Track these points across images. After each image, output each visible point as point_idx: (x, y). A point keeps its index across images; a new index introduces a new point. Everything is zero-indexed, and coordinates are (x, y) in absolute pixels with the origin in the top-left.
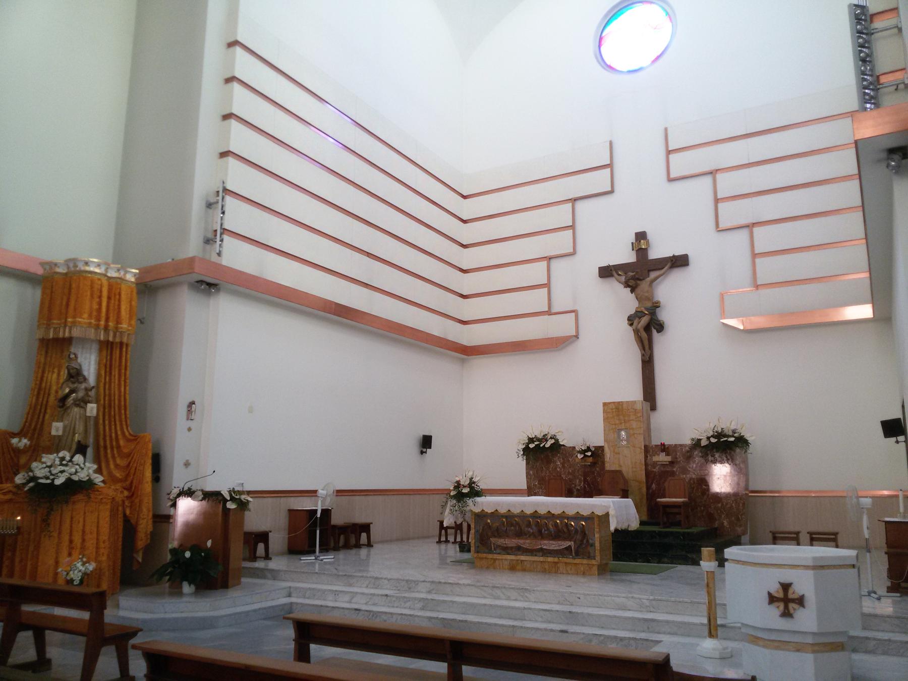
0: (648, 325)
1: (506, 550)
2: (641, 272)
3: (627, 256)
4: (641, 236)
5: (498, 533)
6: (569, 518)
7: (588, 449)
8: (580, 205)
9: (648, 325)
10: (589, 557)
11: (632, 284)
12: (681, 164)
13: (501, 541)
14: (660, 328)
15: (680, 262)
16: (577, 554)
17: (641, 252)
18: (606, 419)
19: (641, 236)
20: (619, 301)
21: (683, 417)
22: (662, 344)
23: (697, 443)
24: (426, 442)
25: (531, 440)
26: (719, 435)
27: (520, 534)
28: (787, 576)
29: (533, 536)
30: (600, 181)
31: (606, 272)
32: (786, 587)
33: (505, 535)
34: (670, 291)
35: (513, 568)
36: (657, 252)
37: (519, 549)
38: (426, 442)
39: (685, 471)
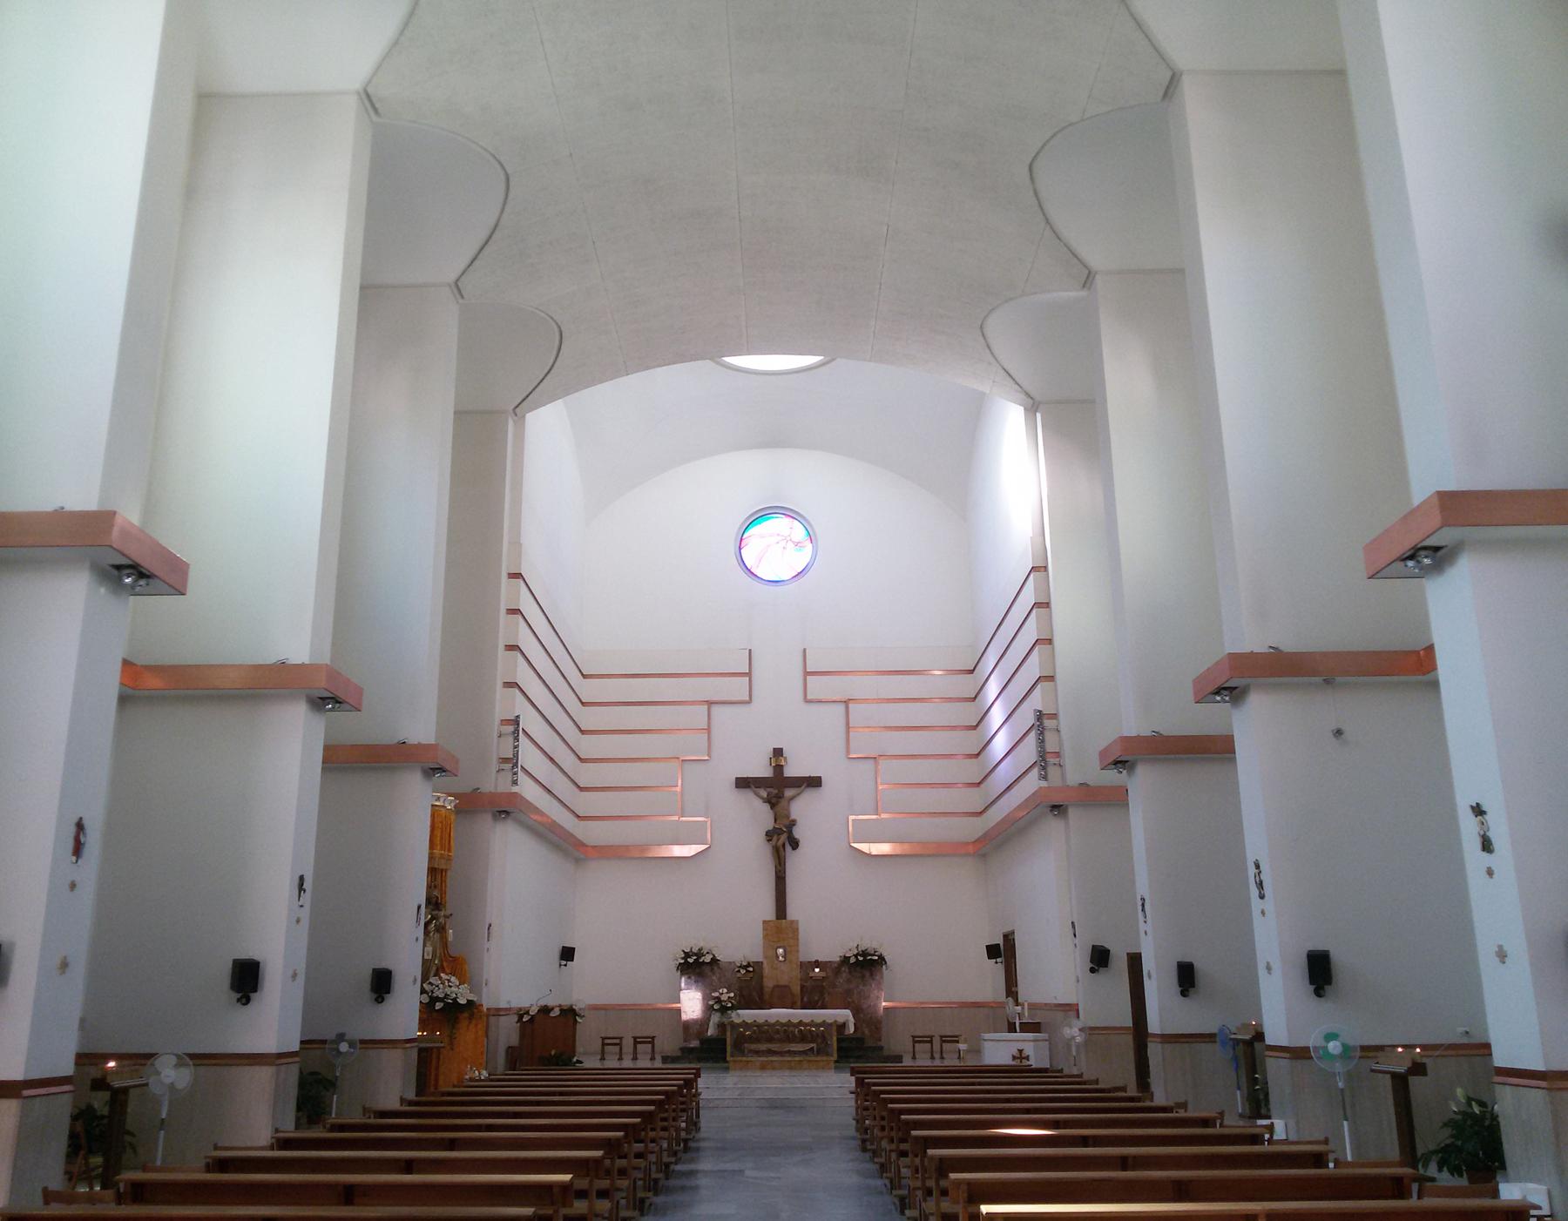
0: (783, 839)
1: (757, 1053)
2: (777, 787)
3: (762, 770)
4: (778, 752)
5: (751, 1039)
6: (806, 1025)
7: (749, 965)
8: (716, 709)
9: (783, 839)
10: (828, 1055)
11: (774, 802)
12: (817, 686)
13: (753, 1046)
14: (795, 844)
15: (814, 782)
16: (819, 1052)
17: (779, 769)
18: (765, 936)
19: (778, 752)
20: (754, 814)
21: (825, 937)
22: (794, 860)
23: (845, 959)
24: (568, 954)
25: (687, 955)
26: (864, 953)
27: (770, 1040)
28: (1020, 1046)
29: (781, 1041)
30: (737, 688)
31: (743, 783)
32: (1021, 1051)
33: (758, 1041)
34: (803, 808)
35: (763, 1067)
36: (790, 772)
37: (771, 1052)
38: (568, 954)
39: (834, 986)
